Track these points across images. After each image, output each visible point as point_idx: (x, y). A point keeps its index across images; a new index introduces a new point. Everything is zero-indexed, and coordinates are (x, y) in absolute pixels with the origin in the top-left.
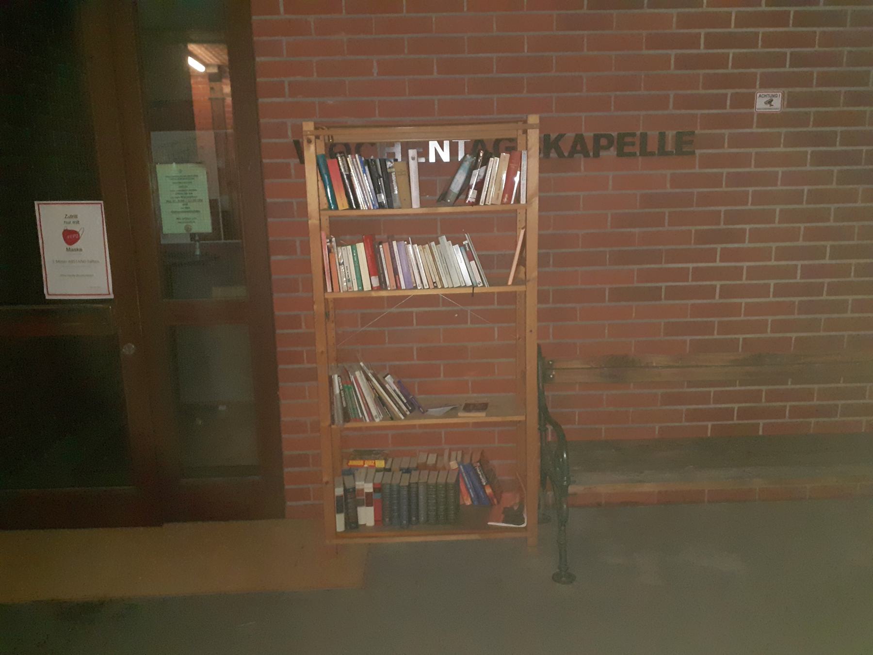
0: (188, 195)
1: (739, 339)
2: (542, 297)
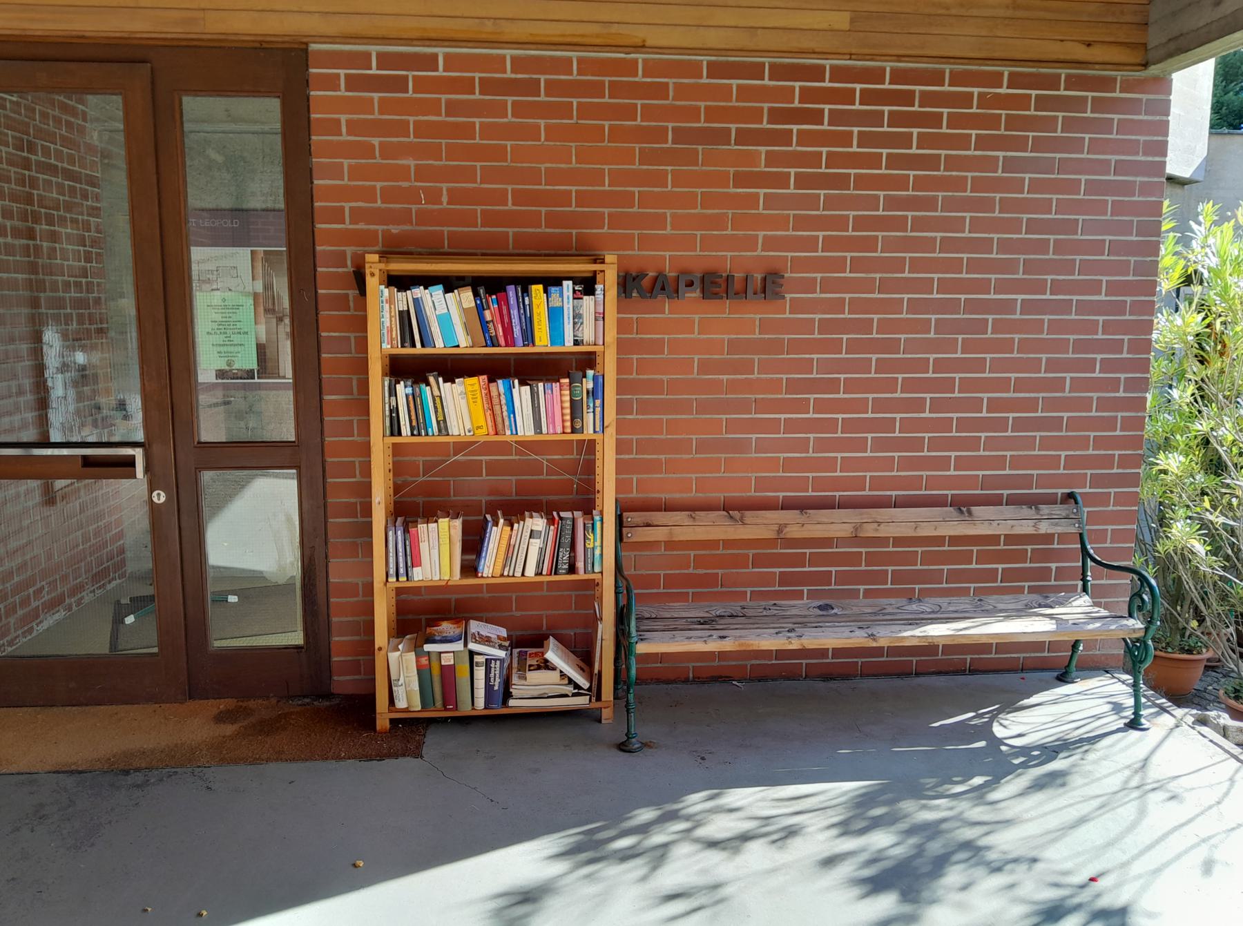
0: (232, 327)
1: (997, 569)
2: (621, 447)
